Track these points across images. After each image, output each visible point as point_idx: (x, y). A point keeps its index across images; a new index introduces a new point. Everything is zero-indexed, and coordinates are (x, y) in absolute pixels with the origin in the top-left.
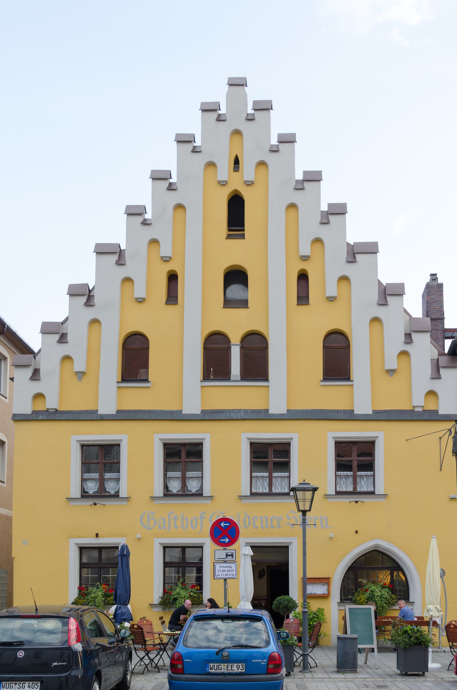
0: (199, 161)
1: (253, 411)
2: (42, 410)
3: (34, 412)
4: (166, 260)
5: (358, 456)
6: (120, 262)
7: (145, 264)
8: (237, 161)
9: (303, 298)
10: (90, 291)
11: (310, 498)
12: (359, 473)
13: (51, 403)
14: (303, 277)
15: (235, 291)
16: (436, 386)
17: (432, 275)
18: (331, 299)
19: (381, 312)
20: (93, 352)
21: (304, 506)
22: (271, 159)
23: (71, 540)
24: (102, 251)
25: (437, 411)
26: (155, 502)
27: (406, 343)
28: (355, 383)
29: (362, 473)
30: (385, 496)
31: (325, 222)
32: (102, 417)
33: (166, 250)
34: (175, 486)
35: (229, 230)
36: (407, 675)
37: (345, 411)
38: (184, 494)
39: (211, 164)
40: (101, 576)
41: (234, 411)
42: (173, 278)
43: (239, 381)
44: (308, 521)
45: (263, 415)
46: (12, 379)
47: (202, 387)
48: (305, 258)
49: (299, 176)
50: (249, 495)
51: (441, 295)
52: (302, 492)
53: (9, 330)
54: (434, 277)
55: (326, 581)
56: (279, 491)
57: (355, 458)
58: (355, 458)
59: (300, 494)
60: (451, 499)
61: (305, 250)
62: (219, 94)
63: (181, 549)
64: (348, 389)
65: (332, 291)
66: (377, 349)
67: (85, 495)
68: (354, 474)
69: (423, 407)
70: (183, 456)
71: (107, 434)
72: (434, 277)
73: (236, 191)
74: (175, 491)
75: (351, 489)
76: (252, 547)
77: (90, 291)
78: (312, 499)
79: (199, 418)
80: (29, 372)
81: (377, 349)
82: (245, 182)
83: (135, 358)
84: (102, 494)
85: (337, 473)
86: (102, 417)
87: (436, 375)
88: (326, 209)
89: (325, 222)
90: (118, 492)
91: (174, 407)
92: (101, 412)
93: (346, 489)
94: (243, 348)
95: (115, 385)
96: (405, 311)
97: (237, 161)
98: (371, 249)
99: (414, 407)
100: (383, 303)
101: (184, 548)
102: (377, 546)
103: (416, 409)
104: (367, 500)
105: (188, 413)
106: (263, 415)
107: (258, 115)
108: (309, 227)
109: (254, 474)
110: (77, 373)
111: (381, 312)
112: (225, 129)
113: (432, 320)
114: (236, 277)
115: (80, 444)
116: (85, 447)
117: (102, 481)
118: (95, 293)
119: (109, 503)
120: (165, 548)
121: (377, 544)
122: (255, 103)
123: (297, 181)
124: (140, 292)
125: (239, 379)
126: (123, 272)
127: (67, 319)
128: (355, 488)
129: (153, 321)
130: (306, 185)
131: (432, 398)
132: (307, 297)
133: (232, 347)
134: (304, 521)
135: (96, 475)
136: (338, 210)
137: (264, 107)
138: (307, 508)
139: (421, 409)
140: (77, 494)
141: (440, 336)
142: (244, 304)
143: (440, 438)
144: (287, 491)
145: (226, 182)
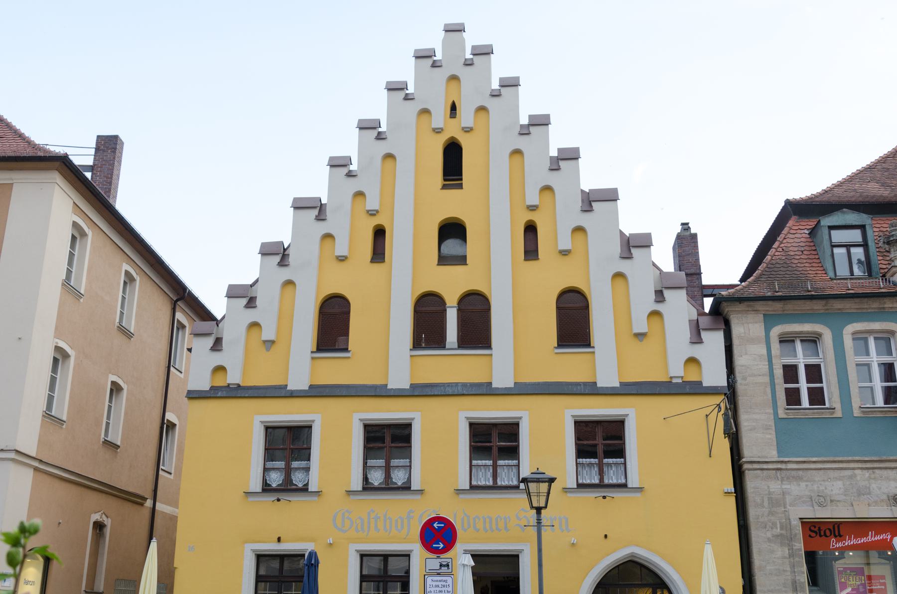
0: (413, 108)
1: (473, 385)
3: (212, 388)
4: (372, 213)
6: (321, 217)
8: (454, 108)
9: (531, 252)
10: (285, 250)
11: (546, 491)
12: (606, 461)
13: (233, 377)
14: (531, 229)
15: (452, 246)
16: (697, 352)
17: (683, 224)
18: (565, 253)
20: (285, 317)
21: (539, 501)
22: (491, 104)
24: (300, 205)
25: (700, 383)
26: (461, 496)
27: (657, 301)
28: (596, 350)
29: (610, 461)
30: (640, 489)
33: (372, 203)
34: (377, 478)
35: (445, 180)
37: (585, 384)
38: (388, 487)
39: (425, 111)
42: (380, 233)
44: (544, 521)
45: (485, 390)
46: (190, 350)
47: (313, 358)
48: (533, 208)
49: (524, 121)
51: (696, 246)
52: (535, 484)
53: (191, 295)
54: (685, 226)
56: (506, 483)
57: (601, 441)
58: (601, 441)
59: (532, 486)
61: (533, 198)
64: (589, 356)
65: (565, 243)
66: (623, 310)
67: (267, 488)
69: (682, 377)
70: (388, 441)
72: (685, 226)
73: (453, 137)
74: (376, 484)
75: (596, 481)
77: (285, 250)
78: (548, 493)
80: (210, 341)
81: (623, 310)
82: (463, 128)
83: (333, 324)
84: (288, 488)
87: (697, 339)
90: (307, 484)
91: (377, 381)
92: (294, 385)
96: (654, 265)
97: (454, 108)
98: (610, 196)
99: (671, 378)
100: (627, 255)
103: (674, 381)
104: (618, 495)
106: (485, 390)
108: (537, 173)
109: (474, 462)
110: (265, 342)
113: (687, 275)
116: (270, 429)
117: (288, 471)
118: (291, 252)
120: (362, 556)
122: (473, 47)
123: (522, 126)
124: (341, 249)
125: (456, 346)
127: (257, 281)
128: (602, 479)
129: (356, 281)
132: (536, 251)
134: (539, 521)
135: (281, 464)
136: (570, 156)
137: (484, 52)
138: (542, 504)
139: (680, 381)
141: (697, 293)
142: (462, 260)
143: (707, 416)
144: (515, 483)
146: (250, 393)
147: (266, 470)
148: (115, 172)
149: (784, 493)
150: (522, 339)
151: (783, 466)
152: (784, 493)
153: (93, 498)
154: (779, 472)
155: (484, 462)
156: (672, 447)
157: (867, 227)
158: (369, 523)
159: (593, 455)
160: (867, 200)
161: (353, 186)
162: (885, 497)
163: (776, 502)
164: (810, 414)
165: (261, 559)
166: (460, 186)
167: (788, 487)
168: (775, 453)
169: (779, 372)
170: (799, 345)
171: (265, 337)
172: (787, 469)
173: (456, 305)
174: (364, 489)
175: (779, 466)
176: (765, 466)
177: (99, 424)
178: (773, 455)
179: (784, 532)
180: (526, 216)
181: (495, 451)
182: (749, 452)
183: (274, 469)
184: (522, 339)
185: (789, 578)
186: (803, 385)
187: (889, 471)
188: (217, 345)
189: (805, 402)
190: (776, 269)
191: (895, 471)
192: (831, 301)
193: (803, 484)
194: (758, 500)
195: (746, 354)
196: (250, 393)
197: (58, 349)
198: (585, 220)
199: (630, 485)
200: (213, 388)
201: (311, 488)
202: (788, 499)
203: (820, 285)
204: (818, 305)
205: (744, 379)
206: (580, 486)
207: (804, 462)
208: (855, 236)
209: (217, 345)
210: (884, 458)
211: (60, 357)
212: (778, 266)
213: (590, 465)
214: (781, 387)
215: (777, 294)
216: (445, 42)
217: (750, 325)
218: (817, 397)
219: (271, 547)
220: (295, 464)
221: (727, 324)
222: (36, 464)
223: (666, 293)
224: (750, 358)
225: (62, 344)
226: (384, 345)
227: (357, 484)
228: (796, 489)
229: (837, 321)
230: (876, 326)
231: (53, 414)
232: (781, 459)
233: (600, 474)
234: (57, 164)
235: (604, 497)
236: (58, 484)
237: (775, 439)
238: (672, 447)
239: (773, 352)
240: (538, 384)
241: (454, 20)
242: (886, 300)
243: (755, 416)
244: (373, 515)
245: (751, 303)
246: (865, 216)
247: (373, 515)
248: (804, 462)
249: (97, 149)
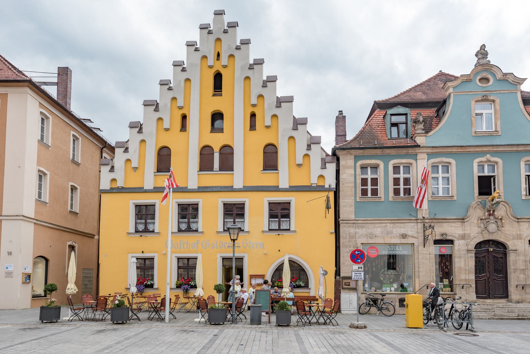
0: (199, 55)
1: (225, 187)
3: (111, 188)
4: (181, 108)
5: (281, 210)
6: (157, 110)
8: (218, 55)
9: (253, 127)
10: (141, 125)
12: (281, 219)
14: (253, 115)
17: (339, 111)
18: (268, 127)
20: (142, 157)
22: (236, 53)
23: (130, 255)
26: (130, 236)
27: (307, 150)
28: (280, 172)
29: (284, 219)
31: (264, 85)
33: (180, 103)
35: (215, 92)
36: (279, 326)
37: (274, 187)
39: (205, 57)
41: (215, 187)
42: (184, 117)
44: (236, 245)
45: (230, 189)
48: (254, 106)
49: (252, 62)
54: (341, 112)
57: (280, 212)
58: (280, 212)
61: (254, 101)
62: (209, 19)
64: (231, 176)
65: (268, 122)
66: (292, 153)
70: (188, 213)
72: (341, 112)
73: (218, 70)
74: (141, 230)
76: (137, 259)
80: (109, 168)
81: (292, 153)
82: (223, 66)
83: (164, 160)
84: (146, 230)
87: (324, 167)
89: (264, 85)
92: (190, 187)
95: (197, 173)
96: (308, 132)
97: (218, 55)
98: (290, 100)
100: (295, 128)
101: (188, 259)
103: (313, 185)
104: (286, 234)
107: (230, 30)
108: (256, 89)
109: (226, 220)
110: (134, 168)
111: (294, 133)
112: (212, 38)
114: (217, 116)
117: (146, 224)
118: (143, 126)
119: (149, 235)
120: (178, 259)
123: (250, 64)
124: (166, 125)
125: (218, 170)
126: (158, 115)
127: (128, 141)
129: (173, 140)
130: (255, 66)
131: (321, 179)
135: (143, 221)
137: (233, 25)
139: (315, 185)
140: (133, 231)
142: (221, 130)
145: (213, 66)
146: (128, 190)
148: (69, 86)
149: (356, 233)
150: (246, 168)
151: (356, 222)
152: (356, 233)
153: (67, 235)
157: (408, 115)
159: (276, 217)
160: (413, 101)
161: (171, 94)
162: (398, 235)
163: (352, 237)
164: (370, 200)
166: (221, 95)
168: (353, 216)
169: (359, 181)
170: (369, 169)
175: (355, 222)
176: (349, 222)
177: (66, 203)
178: (353, 217)
180: (251, 110)
181: (234, 215)
184: (246, 168)
186: (402, 187)
187: (402, 224)
188: (112, 169)
189: (402, 194)
192: (385, 150)
193: (364, 229)
194: (345, 236)
196: (128, 190)
197: (39, 171)
198: (277, 111)
200: (111, 188)
201: (156, 231)
202: (357, 235)
203: (382, 142)
204: (379, 152)
205: (343, 184)
206: (137, 231)
208: (402, 119)
210: (400, 218)
211: (41, 176)
214: (359, 188)
216: (214, 21)
218: (375, 192)
219: (141, 255)
220: (149, 221)
221: (338, 159)
222: (35, 221)
223: (312, 146)
224: (347, 175)
225: (41, 169)
226: (187, 169)
227: (176, 230)
228: (361, 231)
229: (386, 158)
230: (404, 161)
231: (42, 200)
234: (27, 84)
236: (47, 229)
240: (253, 187)
241: (219, 8)
242: (410, 149)
243: (347, 201)
245: (349, 150)
246: (407, 109)
249: (59, 74)
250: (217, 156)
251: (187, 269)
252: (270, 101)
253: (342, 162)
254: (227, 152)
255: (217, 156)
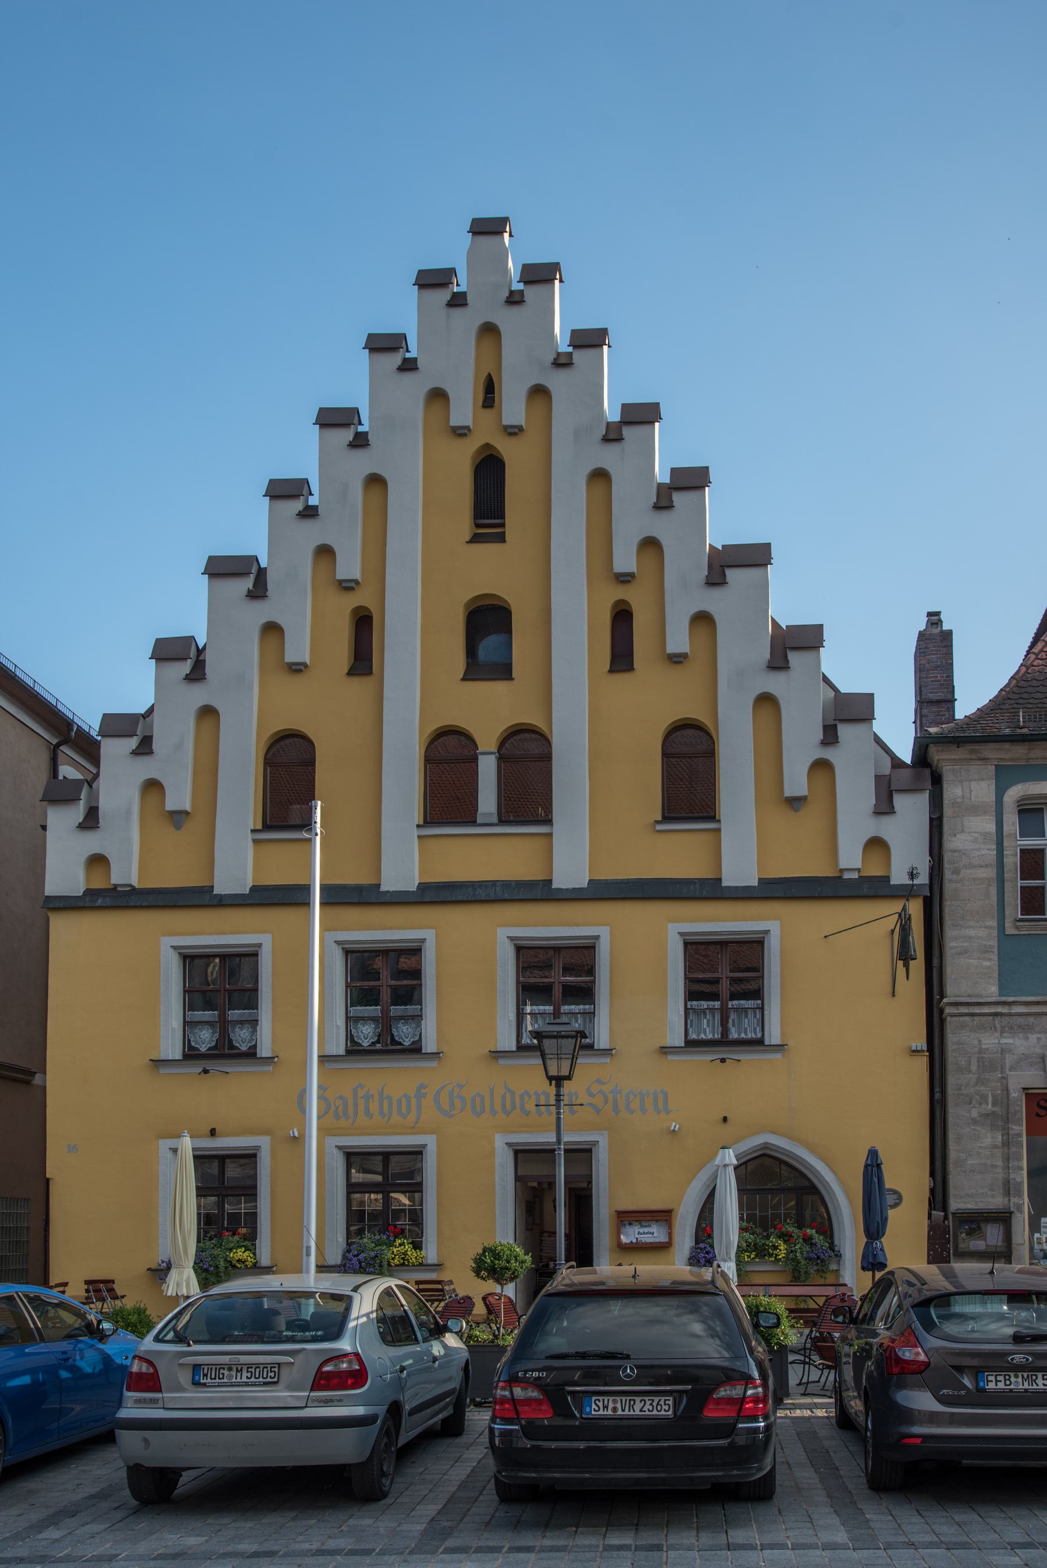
0: (416, 386)
2: (216, 873)
4: (347, 586)
6: (259, 592)
7: (297, 596)
9: (622, 658)
13: (126, 872)
18: (677, 659)
19: (775, 684)
21: (559, 1068)
23: (161, 1142)
24: (220, 569)
25: (887, 879)
30: (437, 1054)
32: (221, 900)
33: (349, 566)
34: (366, 1033)
35: (478, 526)
37: (702, 881)
40: (223, 1210)
41: (473, 885)
43: (496, 825)
47: (419, 837)
48: (625, 579)
50: (514, 1049)
54: (934, 619)
55: (664, 1216)
60: (914, 1051)
61: (625, 560)
63: (381, 1157)
65: (679, 640)
67: (191, 1054)
68: (722, 1004)
69: (859, 870)
71: (231, 933)
72: (934, 619)
77: (200, 652)
79: (414, 900)
80: (77, 812)
84: (390, 1047)
85: (689, 1003)
86: (221, 900)
87: (884, 807)
88: (667, 480)
90: (255, 1046)
93: (698, 1036)
94: (503, 758)
96: (826, 680)
98: (757, 557)
99: (842, 871)
100: (778, 663)
102: (766, 1146)
104: (749, 1057)
105: (391, 890)
111: (775, 684)
115: (180, 954)
116: (190, 959)
117: (223, 1027)
119: (236, 1068)
121: (766, 1143)
124: (298, 649)
127: (151, 710)
129: (322, 710)
130: (626, 431)
132: (630, 655)
133: (480, 757)
134: (558, 1096)
136: (692, 480)
138: (565, 1072)
139: (855, 876)
142: (503, 671)
147: (188, 1025)
154: (998, 1019)
155: (541, 1007)
156: (835, 980)
158: (356, 1105)
163: (991, 1064)
165: (353, 1159)
166: (501, 538)
167: (1011, 1041)
168: (994, 989)
169: (1013, 860)
171: (170, 805)
172: (1010, 1015)
173: (494, 749)
174: (349, 1052)
175: (1000, 1009)
176: (977, 1010)
179: (997, 1109)
181: (557, 991)
182: (955, 989)
183: (402, 1018)
185: (1000, 1176)
188: (91, 820)
190: (1030, 690)
191: (1045, 1018)
193: (1033, 1037)
194: (963, 1062)
195: (963, 831)
199: (766, 1043)
201: (264, 1051)
202: (1009, 1060)
205: (956, 872)
206: (692, 1044)
207: (1038, 1003)
209: (91, 820)
212: (1034, 683)
213: (712, 1010)
214: (1015, 884)
215: (1019, 731)
217: (973, 784)
220: (234, 1014)
221: (937, 780)
224: (972, 838)
228: (1021, 1044)
232: (1003, 999)
233: (722, 1025)
235: (723, 1060)
237: (996, 968)
238: (835, 980)
239: (1005, 828)
243: (971, 933)
244: (361, 1093)
245: (976, 747)
247: (361, 1093)
248: (1038, 1003)
250: (487, 768)
251: (384, 1197)
252: (682, 570)
253: (952, 791)
254: (527, 757)
255: (487, 768)
